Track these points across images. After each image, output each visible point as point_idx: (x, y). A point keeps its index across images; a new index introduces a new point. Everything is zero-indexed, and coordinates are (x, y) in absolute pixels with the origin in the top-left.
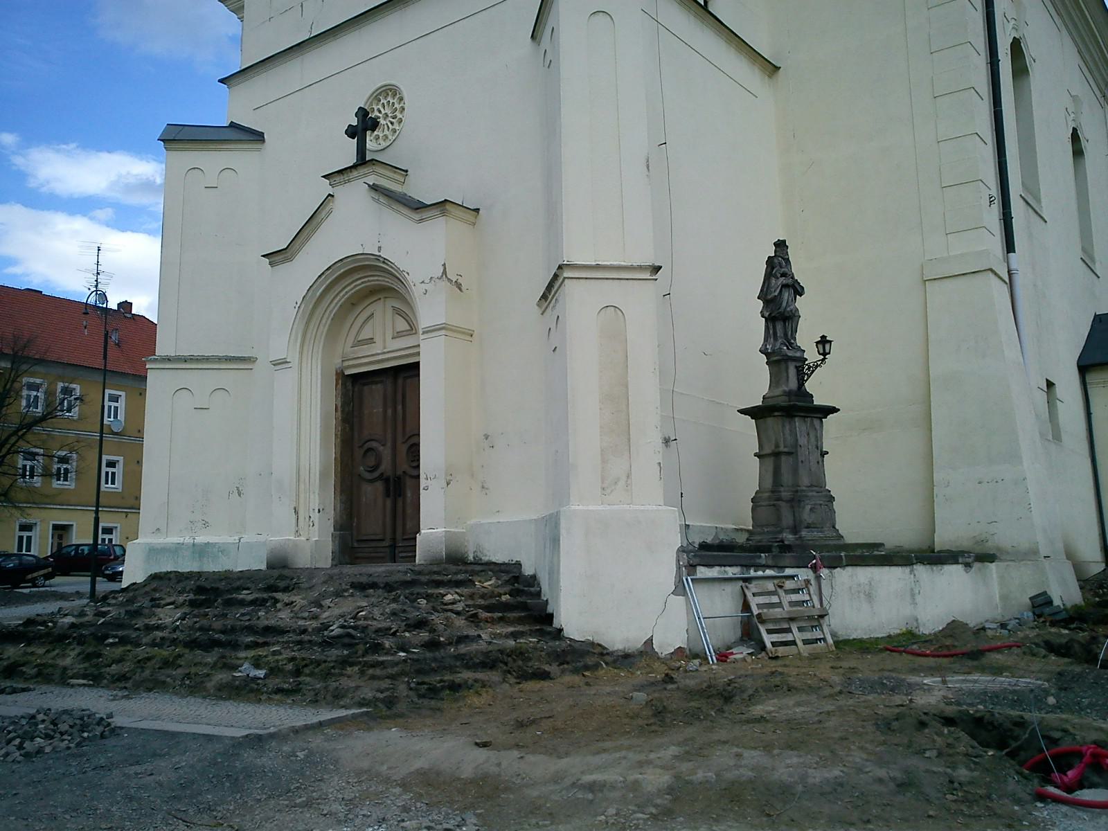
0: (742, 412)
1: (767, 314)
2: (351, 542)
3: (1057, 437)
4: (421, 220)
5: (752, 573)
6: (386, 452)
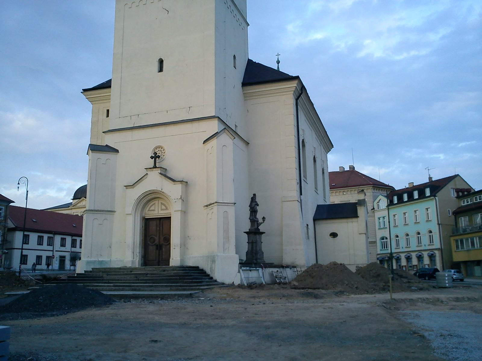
0: (244, 232)
1: (251, 210)
2: (146, 261)
3: (308, 238)
4: (175, 184)
5: (251, 269)
6: (157, 238)
